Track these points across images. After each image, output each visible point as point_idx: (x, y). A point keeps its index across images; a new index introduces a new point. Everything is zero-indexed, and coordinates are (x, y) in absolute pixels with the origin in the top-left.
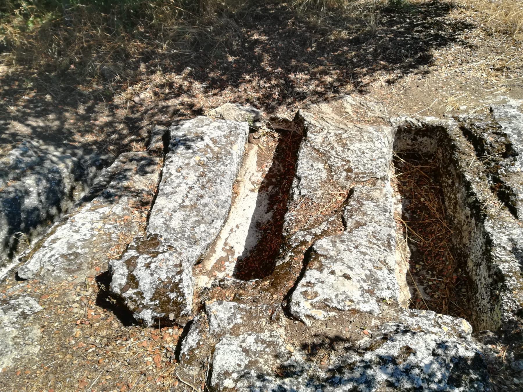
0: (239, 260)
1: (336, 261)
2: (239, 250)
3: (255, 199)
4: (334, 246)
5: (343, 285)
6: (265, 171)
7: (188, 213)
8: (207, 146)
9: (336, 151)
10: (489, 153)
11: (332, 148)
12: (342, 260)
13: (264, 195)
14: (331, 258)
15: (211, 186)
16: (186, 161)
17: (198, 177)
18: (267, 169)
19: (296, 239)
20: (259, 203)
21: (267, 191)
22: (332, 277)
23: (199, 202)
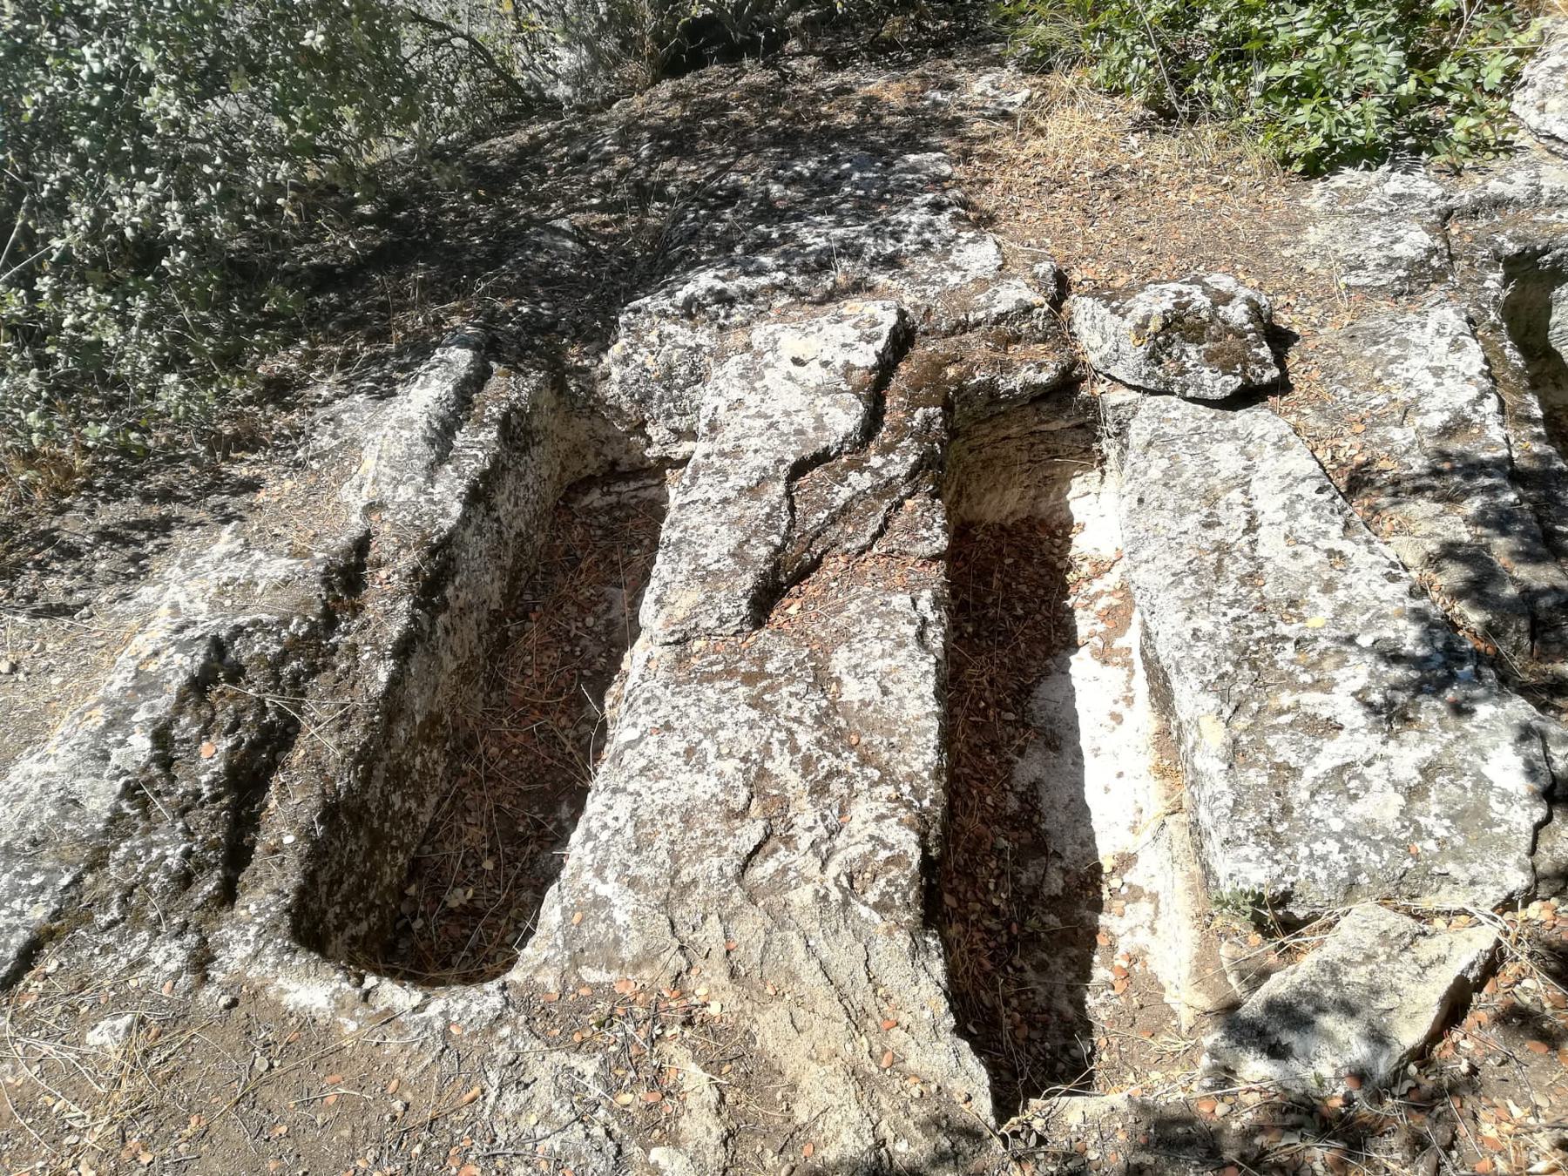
0: (1072, 645)
2: (1081, 666)
3: (1097, 823)
4: (819, 418)
6: (1108, 963)
7: (1212, 481)
9: (795, 749)
10: (264, 711)
11: (808, 764)
16: (1341, 595)
18: (1100, 973)
19: (904, 454)
20: (1080, 812)
21: (1066, 871)
22: (826, 357)
23: (1205, 511)
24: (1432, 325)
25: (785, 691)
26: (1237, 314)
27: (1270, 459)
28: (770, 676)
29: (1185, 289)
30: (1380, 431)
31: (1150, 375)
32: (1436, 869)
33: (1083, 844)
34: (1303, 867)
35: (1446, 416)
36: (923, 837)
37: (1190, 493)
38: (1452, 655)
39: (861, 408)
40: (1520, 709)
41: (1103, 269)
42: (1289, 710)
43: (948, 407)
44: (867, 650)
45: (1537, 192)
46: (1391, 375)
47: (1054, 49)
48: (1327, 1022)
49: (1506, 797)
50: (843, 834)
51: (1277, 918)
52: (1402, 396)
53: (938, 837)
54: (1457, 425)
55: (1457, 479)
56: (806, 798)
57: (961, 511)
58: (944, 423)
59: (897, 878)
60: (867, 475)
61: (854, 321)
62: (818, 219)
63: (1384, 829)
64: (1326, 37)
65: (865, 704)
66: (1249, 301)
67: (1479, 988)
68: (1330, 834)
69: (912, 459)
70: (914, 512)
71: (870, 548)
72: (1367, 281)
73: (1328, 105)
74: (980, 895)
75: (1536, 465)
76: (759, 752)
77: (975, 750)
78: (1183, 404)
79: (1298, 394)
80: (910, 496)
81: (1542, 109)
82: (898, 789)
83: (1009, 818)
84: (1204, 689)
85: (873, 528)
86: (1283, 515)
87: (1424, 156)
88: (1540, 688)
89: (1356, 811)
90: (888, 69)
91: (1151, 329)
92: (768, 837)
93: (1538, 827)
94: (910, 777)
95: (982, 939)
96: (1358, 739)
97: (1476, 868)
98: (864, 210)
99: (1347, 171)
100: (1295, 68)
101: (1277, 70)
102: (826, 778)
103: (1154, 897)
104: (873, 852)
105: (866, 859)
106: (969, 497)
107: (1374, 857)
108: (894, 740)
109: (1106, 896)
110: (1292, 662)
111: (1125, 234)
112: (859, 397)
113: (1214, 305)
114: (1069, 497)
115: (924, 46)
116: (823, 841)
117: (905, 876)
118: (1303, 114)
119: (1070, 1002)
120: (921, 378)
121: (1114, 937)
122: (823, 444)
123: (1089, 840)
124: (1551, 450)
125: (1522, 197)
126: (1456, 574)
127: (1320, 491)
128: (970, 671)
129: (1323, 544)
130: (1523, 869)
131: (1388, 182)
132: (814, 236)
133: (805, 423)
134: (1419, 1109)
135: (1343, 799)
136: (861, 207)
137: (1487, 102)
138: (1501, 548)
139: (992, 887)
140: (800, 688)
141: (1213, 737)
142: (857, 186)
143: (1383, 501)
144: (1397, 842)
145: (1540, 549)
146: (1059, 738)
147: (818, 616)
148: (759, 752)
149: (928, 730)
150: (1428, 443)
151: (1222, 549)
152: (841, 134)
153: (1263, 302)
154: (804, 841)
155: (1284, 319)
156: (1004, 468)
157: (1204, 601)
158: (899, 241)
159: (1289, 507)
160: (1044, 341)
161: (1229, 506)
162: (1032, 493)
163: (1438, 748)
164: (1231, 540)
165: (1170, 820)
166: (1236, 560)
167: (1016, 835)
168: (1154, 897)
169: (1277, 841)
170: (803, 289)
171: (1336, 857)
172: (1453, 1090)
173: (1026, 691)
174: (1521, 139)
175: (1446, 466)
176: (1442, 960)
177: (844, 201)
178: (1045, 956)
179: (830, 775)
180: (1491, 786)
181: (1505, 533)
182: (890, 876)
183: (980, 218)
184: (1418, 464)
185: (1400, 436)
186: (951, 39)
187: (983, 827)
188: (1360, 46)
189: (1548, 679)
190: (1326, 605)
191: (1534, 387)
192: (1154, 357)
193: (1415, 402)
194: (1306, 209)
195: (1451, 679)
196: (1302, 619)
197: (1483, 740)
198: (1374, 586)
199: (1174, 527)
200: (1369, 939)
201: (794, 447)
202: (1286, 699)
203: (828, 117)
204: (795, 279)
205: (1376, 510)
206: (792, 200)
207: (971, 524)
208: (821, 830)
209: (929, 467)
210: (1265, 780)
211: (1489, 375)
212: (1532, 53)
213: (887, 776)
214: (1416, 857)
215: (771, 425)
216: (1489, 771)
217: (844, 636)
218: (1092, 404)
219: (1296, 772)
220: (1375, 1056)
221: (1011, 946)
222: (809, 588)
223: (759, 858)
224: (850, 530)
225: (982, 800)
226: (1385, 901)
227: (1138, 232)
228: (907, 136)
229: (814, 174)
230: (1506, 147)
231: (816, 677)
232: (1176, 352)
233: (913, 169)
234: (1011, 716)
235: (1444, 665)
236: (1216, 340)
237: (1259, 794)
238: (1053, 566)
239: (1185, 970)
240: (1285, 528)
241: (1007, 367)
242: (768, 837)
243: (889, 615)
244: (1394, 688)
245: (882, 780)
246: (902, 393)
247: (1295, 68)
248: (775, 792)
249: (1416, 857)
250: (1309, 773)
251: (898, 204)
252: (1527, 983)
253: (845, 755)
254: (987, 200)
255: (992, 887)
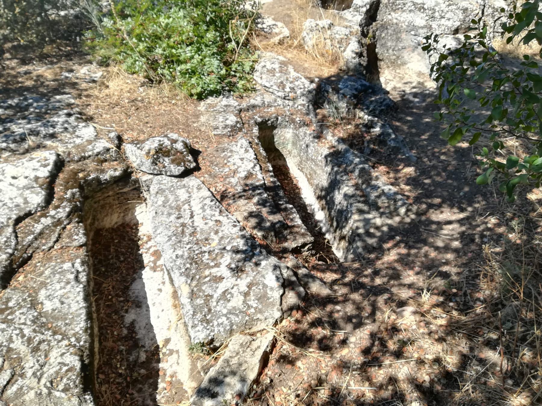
0: (143, 267)
1: (24, 187)
2: (146, 274)
3: (156, 330)
4: (25, 199)
5: (18, 171)
7: (178, 203)
8: (217, 265)
9: (23, 336)
12: (19, 189)
13: (148, 343)
14: (28, 189)
15: (176, 230)
16: (220, 234)
17: (196, 229)
18: (161, 385)
20: (149, 327)
21: (146, 351)
23: (177, 213)
24: (239, 145)
25: (17, 313)
26: (179, 146)
27: (195, 193)
28: (11, 308)
29: (162, 139)
30: (228, 180)
31: (155, 169)
32: (255, 318)
33: (152, 340)
34: (216, 329)
35: (246, 173)
36: (81, 357)
37: (171, 208)
38: (253, 247)
39: (43, 193)
40: (273, 260)
41: (135, 134)
42: (208, 276)
43: (81, 188)
44: (53, 288)
45: (264, 103)
46: (229, 162)
47: (109, 58)
48: (228, 380)
49: (272, 289)
50: (47, 366)
51: (211, 347)
52: (233, 168)
53: (88, 355)
54: (249, 175)
55: (251, 192)
56: (29, 355)
57: (96, 225)
58: (81, 195)
59: (71, 376)
60: (49, 218)
61: (37, 160)
62: (20, 121)
63: (239, 309)
64: (196, 56)
65: (53, 310)
66: (183, 142)
67: (271, 353)
68: (223, 315)
69: (68, 210)
70: (71, 230)
71: (53, 247)
72: (220, 133)
73: (200, 78)
74: (114, 371)
75: (272, 185)
76: (7, 341)
77: (109, 316)
78: (167, 178)
79: (203, 171)
80: (68, 224)
81: (261, 78)
82: (70, 341)
83: (123, 338)
84: (181, 275)
85: (54, 239)
86: (201, 211)
87: (232, 93)
88: (279, 252)
89: (230, 305)
90: (46, 64)
91: (151, 153)
92: (13, 376)
93: (282, 296)
94: (74, 335)
95: (116, 388)
96: (229, 281)
97: (266, 314)
98: (39, 117)
99: (210, 98)
100: (188, 66)
101: (183, 67)
102: (38, 344)
103: (177, 352)
104: (61, 369)
105: (57, 373)
106: (98, 220)
107: (237, 319)
108: (67, 321)
109: (161, 356)
110: (208, 259)
111: (141, 121)
112: (42, 189)
113: (172, 144)
114: (136, 214)
115: (61, 56)
116: (38, 371)
117: (74, 375)
118: (193, 81)
119: (151, 400)
120: (69, 179)
121: (165, 370)
122: (28, 209)
123: (154, 338)
124: (276, 179)
125: (260, 104)
126: (253, 221)
127: (212, 201)
128: (104, 285)
129: (214, 218)
130: (279, 311)
131: (222, 101)
132: (18, 128)
133: (19, 202)
134: (258, 400)
135: (226, 302)
136: (38, 116)
137: (247, 76)
138: (265, 211)
139: (118, 366)
140: (24, 310)
141: (185, 291)
142: (36, 108)
143: (231, 201)
144: (243, 312)
145: (275, 210)
146: (140, 303)
147: (32, 278)
148: (7, 341)
149: (81, 314)
150: (242, 182)
151: (183, 225)
152: (28, 89)
153: (188, 141)
154: (29, 373)
155: (196, 147)
156: (110, 207)
157: (179, 244)
158: (54, 128)
159: (203, 208)
160: (116, 160)
161: (185, 210)
162: (122, 215)
163: (252, 278)
164: (186, 222)
165: (179, 323)
166: (188, 228)
167: (127, 343)
168: (177, 352)
169: (208, 322)
170: (15, 149)
171: (226, 322)
172: (267, 390)
173: (127, 288)
174: (258, 87)
175: (247, 188)
176: (259, 347)
177: (31, 114)
178: (141, 386)
179: (40, 343)
180: (267, 287)
181: (265, 206)
182: (68, 377)
183: (87, 118)
184: (239, 189)
185: (234, 181)
186: (72, 54)
187: (114, 344)
188: (207, 59)
189: (281, 249)
190: (216, 238)
191: (269, 161)
192: (154, 163)
193: (237, 169)
194: (199, 111)
195: (254, 255)
196: (210, 244)
197: (264, 272)
198: (230, 230)
199: (167, 220)
200: (237, 347)
201: (15, 212)
202: (207, 272)
203: (21, 83)
204: (11, 146)
205: (229, 205)
206: (8, 115)
207: (101, 230)
208: (37, 366)
209: (76, 212)
210: (203, 302)
211: (256, 159)
212: (257, 61)
213: (65, 336)
214: (249, 315)
215: (4, 205)
216: (266, 282)
217: (44, 285)
218: (137, 181)
219: (212, 296)
220: (243, 386)
221: (128, 386)
222: (27, 268)
223: (9, 386)
224: (44, 241)
225: (112, 333)
226: (242, 332)
227: (146, 120)
228: (55, 89)
229: (17, 104)
230: (254, 90)
231: (32, 304)
232: (161, 160)
233: (59, 101)
234: (122, 299)
235: (252, 251)
236: (174, 155)
237: (201, 307)
238: (133, 240)
239: (187, 375)
240: (202, 215)
241: (103, 171)
242: (13, 376)
243: (63, 272)
244: (238, 261)
245: (63, 339)
246: (61, 185)
247: (188, 66)
248: (15, 356)
249: (249, 315)
250: (216, 296)
251: (53, 114)
252: (284, 347)
253: (46, 332)
254: (90, 111)
255: (118, 366)
